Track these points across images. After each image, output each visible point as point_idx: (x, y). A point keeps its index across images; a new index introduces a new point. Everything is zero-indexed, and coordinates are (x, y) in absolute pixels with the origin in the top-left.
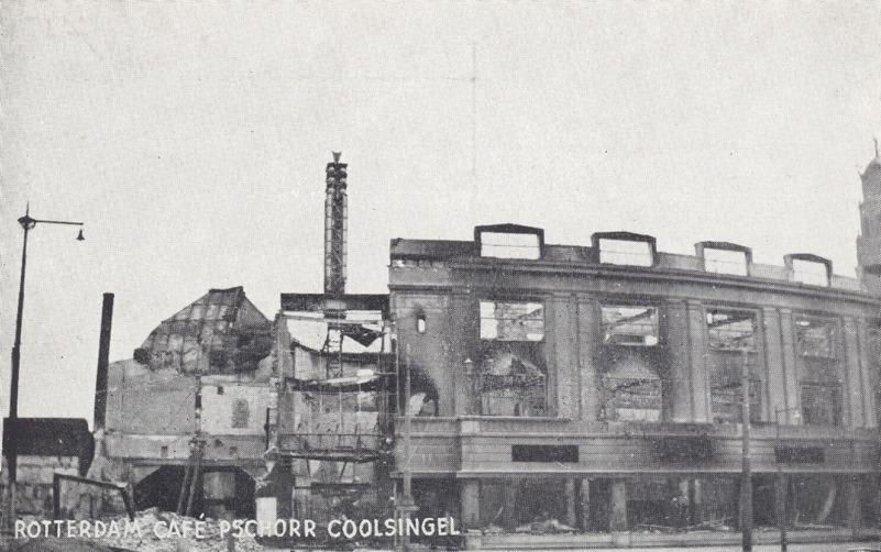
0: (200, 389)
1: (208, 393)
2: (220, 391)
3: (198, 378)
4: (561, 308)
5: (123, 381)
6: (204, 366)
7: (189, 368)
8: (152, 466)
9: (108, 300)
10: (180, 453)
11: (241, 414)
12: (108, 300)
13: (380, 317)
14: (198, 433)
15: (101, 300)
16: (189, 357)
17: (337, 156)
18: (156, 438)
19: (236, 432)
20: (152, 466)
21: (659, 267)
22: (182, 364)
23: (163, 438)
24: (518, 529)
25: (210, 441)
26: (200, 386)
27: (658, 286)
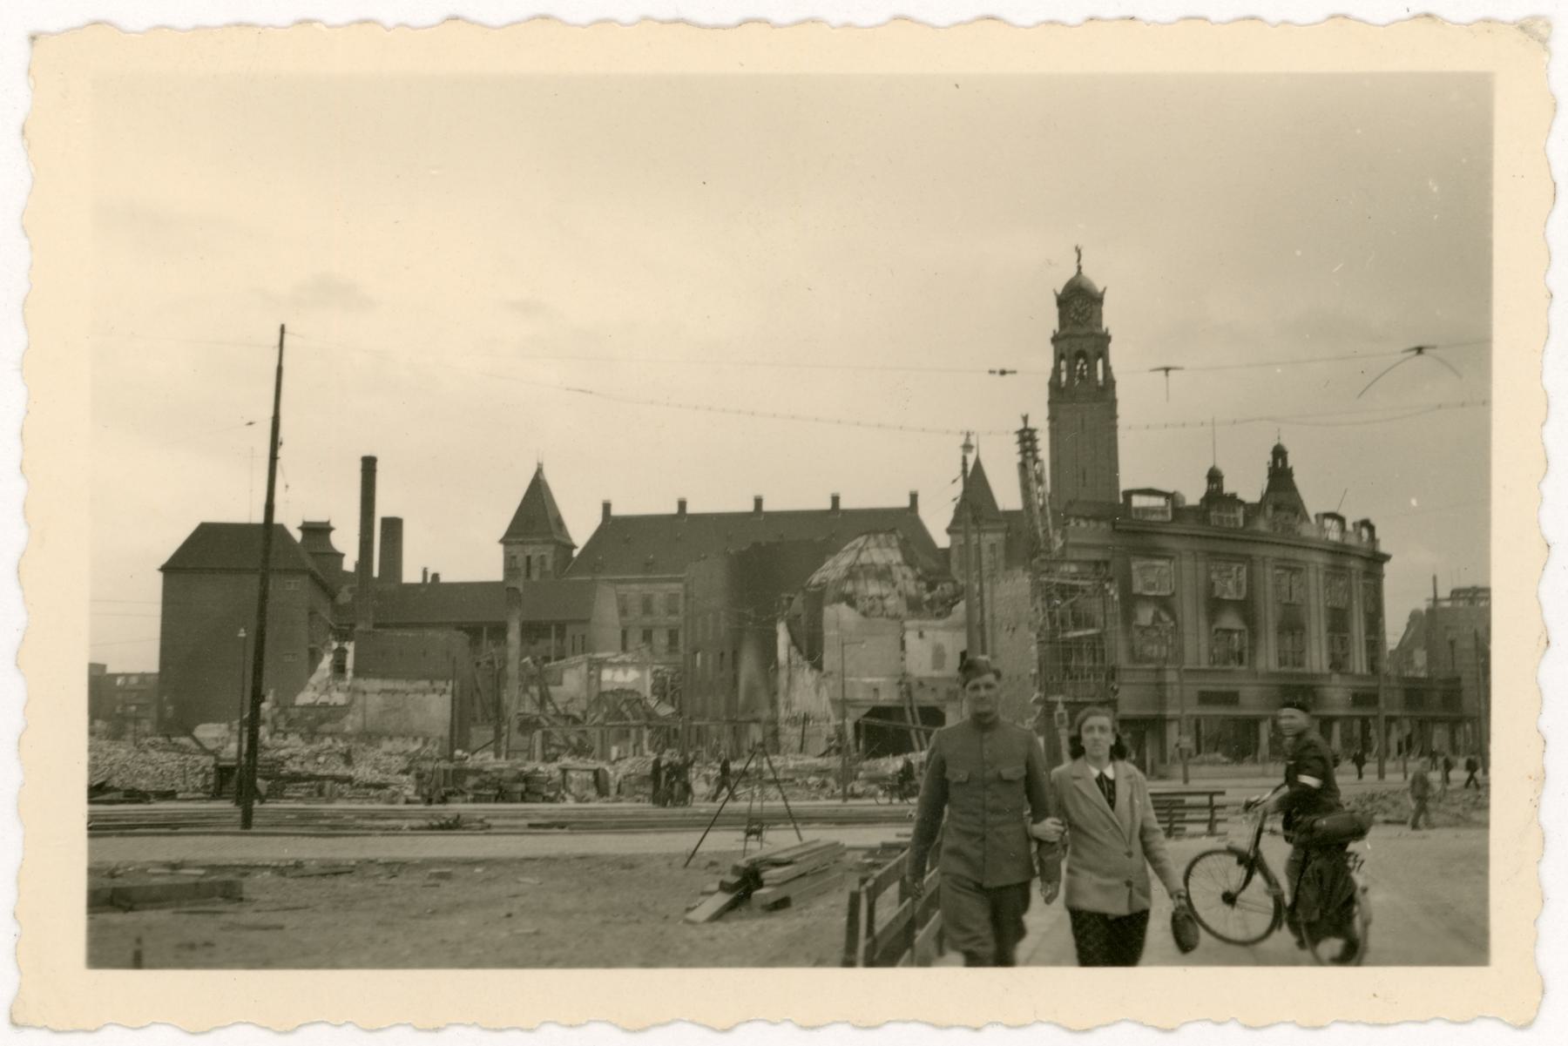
0: (904, 633)
1: (911, 637)
2: (921, 635)
3: (902, 622)
4: (1187, 563)
5: (838, 624)
6: (903, 610)
7: (891, 612)
8: (863, 707)
9: (369, 465)
10: (888, 696)
11: (939, 656)
12: (369, 465)
13: (896, 557)
14: (904, 675)
15: (358, 466)
16: (890, 602)
17: (1025, 419)
18: (868, 680)
19: (936, 673)
20: (863, 707)
21: (1248, 529)
22: (884, 608)
23: (875, 680)
24: (1159, 502)
25: (915, 685)
26: (904, 630)
27: (305, 828)
